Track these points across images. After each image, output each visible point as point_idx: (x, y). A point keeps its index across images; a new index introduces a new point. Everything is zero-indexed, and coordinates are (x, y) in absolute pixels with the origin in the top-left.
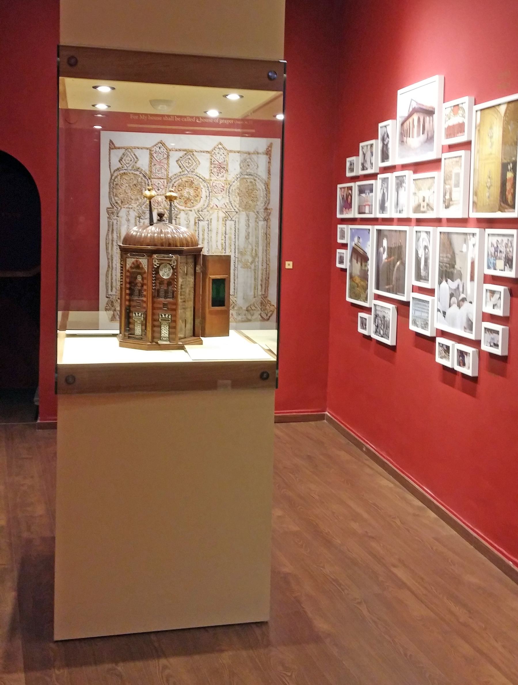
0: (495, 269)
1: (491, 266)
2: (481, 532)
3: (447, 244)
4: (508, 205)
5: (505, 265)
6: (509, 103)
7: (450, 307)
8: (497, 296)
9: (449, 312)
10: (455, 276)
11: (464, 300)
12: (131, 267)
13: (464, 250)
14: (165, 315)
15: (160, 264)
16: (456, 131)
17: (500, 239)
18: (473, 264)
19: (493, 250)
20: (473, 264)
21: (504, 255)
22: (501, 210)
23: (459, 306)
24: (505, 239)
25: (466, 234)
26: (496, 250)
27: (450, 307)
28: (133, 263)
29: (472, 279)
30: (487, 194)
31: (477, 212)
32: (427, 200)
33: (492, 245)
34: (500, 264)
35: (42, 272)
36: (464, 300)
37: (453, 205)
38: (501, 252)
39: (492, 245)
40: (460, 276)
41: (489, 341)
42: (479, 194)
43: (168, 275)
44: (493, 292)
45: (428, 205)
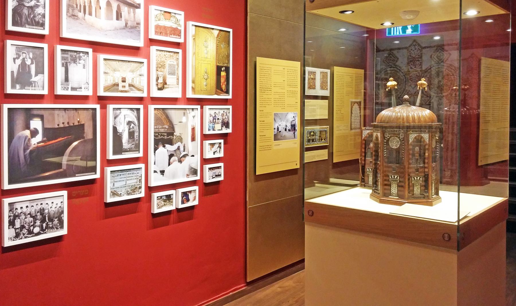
0: (214, 130)
1: (211, 128)
2: (204, 301)
3: (164, 118)
4: (222, 90)
5: (222, 127)
6: (221, 30)
7: (169, 165)
8: (216, 146)
9: (167, 170)
10: (174, 141)
11: (185, 156)
12: (413, 141)
13: (184, 119)
14: (417, 178)
15: (390, 137)
16: (168, 32)
17: (217, 111)
18: (193, 129)
19: (212, 119)
20: (193, 129)
21: (221, 121)
22: (216, 93)
23: (180, 161)
24: (222, 112)
25: (185, 109)
26: (214, 119)
27: (169, 165)
28: (415, 138)
29: (193, 139)
30: (205, 83)
31: (195, 94)
32: (129, 81)
33: (211, 115)
34: (218, 126)
35: (455, 270)
36: (185, 156)
37: (166, 88)
38: (218, 119)
39: (211, 115)
40: (180, 139)
41: (212, 175)
42: (196, 82)
43: (396, 146)
44: (213, 145)
45: (130, 85)
